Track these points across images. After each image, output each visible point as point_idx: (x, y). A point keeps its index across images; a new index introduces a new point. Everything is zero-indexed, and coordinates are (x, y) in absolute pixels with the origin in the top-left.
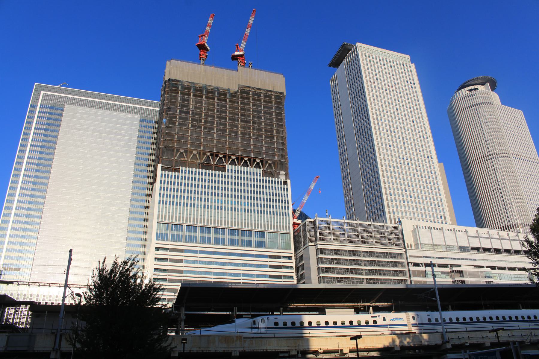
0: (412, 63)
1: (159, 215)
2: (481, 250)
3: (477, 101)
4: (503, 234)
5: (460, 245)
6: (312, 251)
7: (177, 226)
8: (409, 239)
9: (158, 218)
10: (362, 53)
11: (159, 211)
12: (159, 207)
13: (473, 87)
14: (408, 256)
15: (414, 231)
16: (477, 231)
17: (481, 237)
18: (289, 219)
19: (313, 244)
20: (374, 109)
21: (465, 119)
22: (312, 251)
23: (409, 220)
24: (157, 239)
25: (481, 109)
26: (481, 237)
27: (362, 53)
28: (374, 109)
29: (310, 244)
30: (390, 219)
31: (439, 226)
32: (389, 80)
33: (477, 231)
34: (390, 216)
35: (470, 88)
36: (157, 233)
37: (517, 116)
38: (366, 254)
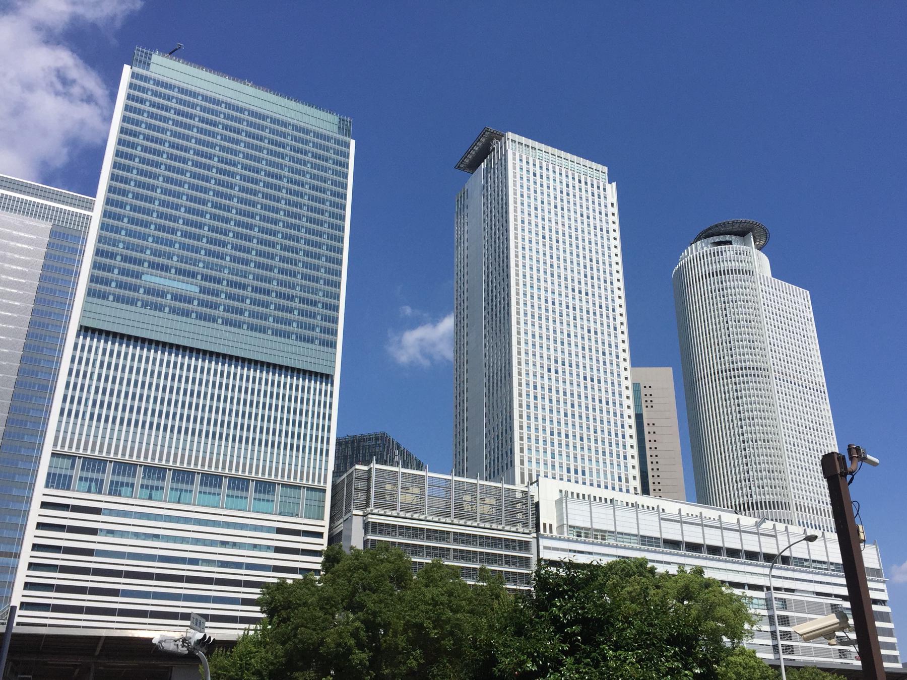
0: (610, 182)
1: (57, 438)
2: (683, 546)
3: (723, 266)
4: (748, 521)
5: (642, 533)
6: (357, 525)
7: (94, 464)
8: (547, 516)
9: (55, 445)
10: (514, 154)
11: (58, 431)
12: (60, 422)
13: (721, 238)
14: (541, 548)
15: (559, 502)
16: (738, 519)
17: (706, 526)
18: (327, 461)
19: (361, 513)
20: (521, 265)
21: (699, 296)
22: (357, 525)
23: (549, 480)
24: (47, 486)
25: (732, 282)
26: (706, 526)
27: (514, 154)
28: (521, 265)
29: (355, 512)
30: (522, 474)
31: (609, 494)
32: (558, 213)
33: (738, 519)
34: (522, 469)
35: (717, 239)
36: (49, 474)
37: (798, 302)
38: (460, 538)
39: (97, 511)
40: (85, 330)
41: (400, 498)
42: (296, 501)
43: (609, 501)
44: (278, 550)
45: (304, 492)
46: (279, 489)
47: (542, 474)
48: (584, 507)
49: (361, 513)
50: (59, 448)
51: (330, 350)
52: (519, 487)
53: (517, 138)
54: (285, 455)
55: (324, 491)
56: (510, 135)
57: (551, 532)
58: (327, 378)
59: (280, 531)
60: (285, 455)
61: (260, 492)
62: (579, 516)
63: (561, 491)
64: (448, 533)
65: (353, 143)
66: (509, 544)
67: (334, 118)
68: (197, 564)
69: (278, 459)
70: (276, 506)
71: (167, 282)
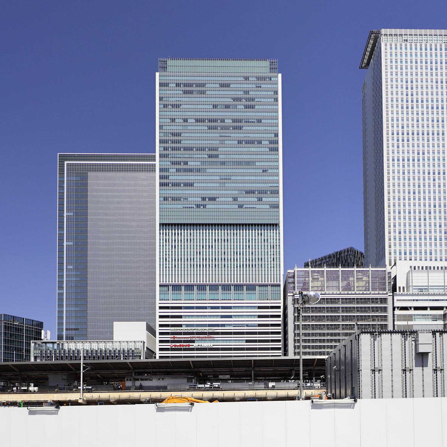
8: (401, 283)
9: (160, 281)
14: (395, 301)
39: (230, 308)
40: (162, 225)
41: (311, 284)
42: (266, 292)
43: (424, 268)
44: (260, 316)
45: (269, 287)
46: (257, 287)
47: (398, 259)
48: (424, 274)
49: (292, 294)
50: (162, 282)
51: (275, 210)
52: (388, 269)
53: (388, 31)
54: (249, 270)
55: (280, 285)
56: (383, 31)
57: (404, 291)
58: (276, 225)
59: (259, 308)
60: (249, 270)
61: (237, 290)
62: (420, 279)
63: (411, 267)
64: (338, 299)
65: (280, 75)
66: (374, 300)
67: (266, 63)
68: (225, 327)
69: (194, 273)
70: (257, 295)
71: (180, 192)
